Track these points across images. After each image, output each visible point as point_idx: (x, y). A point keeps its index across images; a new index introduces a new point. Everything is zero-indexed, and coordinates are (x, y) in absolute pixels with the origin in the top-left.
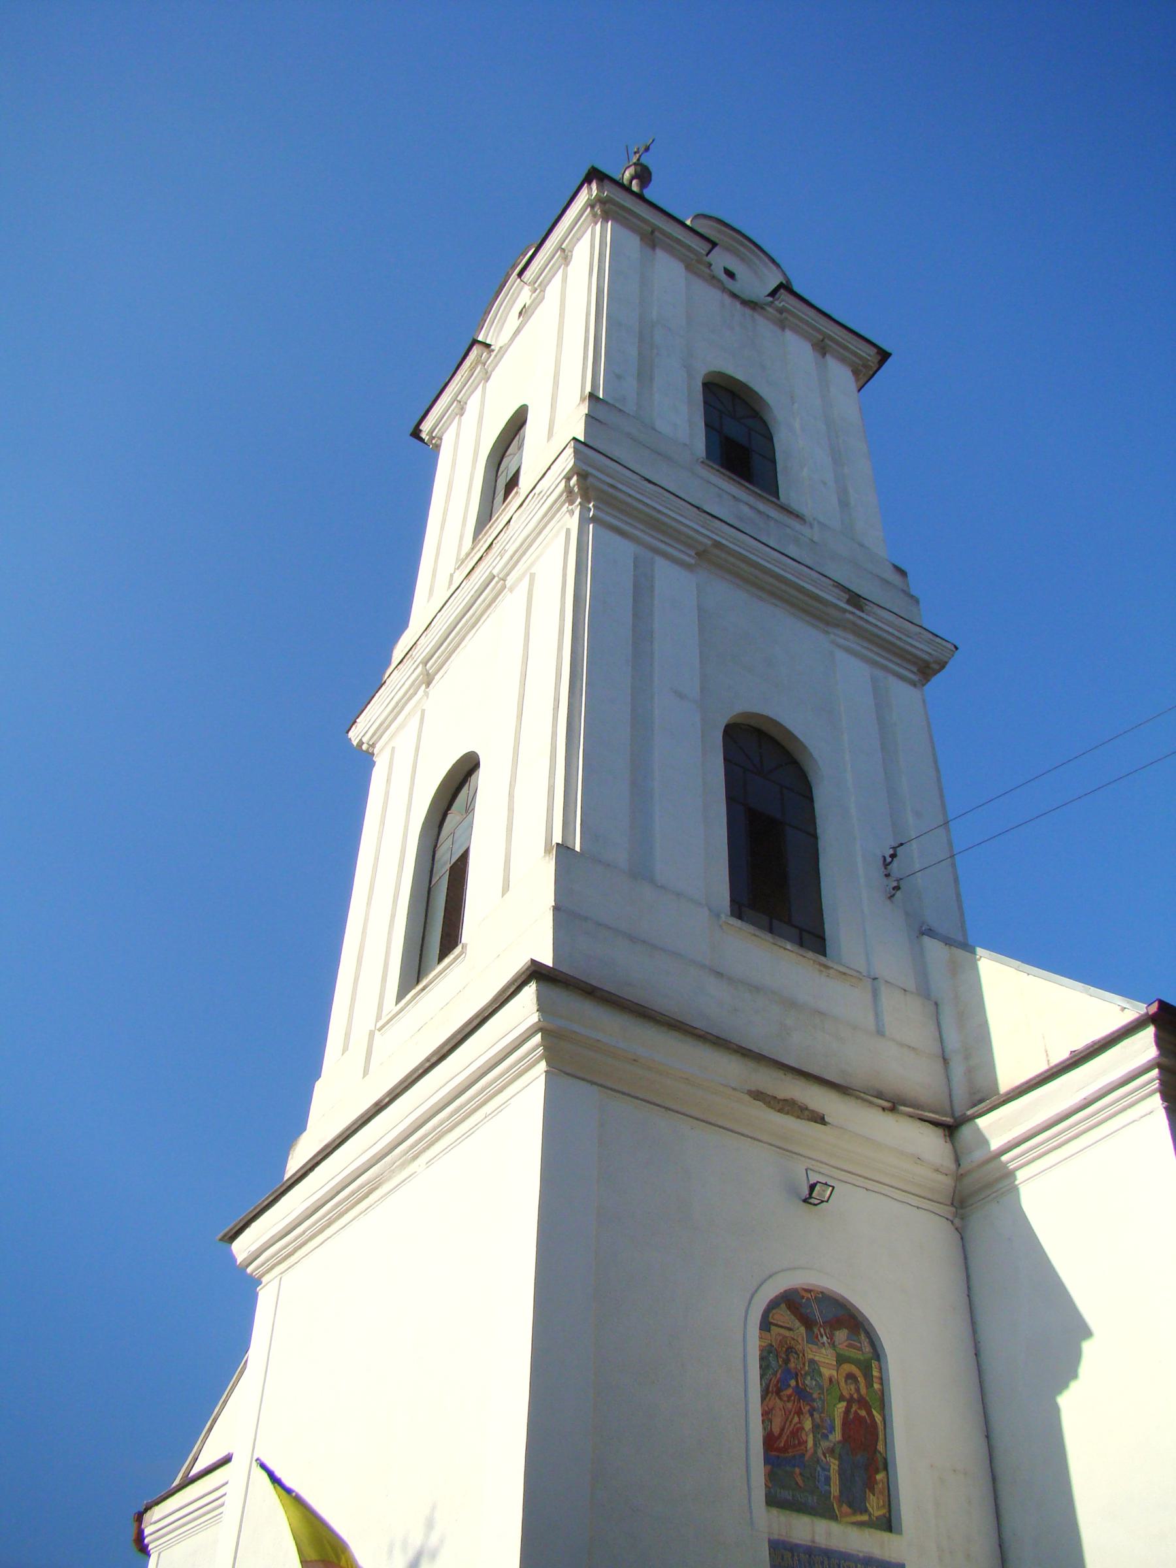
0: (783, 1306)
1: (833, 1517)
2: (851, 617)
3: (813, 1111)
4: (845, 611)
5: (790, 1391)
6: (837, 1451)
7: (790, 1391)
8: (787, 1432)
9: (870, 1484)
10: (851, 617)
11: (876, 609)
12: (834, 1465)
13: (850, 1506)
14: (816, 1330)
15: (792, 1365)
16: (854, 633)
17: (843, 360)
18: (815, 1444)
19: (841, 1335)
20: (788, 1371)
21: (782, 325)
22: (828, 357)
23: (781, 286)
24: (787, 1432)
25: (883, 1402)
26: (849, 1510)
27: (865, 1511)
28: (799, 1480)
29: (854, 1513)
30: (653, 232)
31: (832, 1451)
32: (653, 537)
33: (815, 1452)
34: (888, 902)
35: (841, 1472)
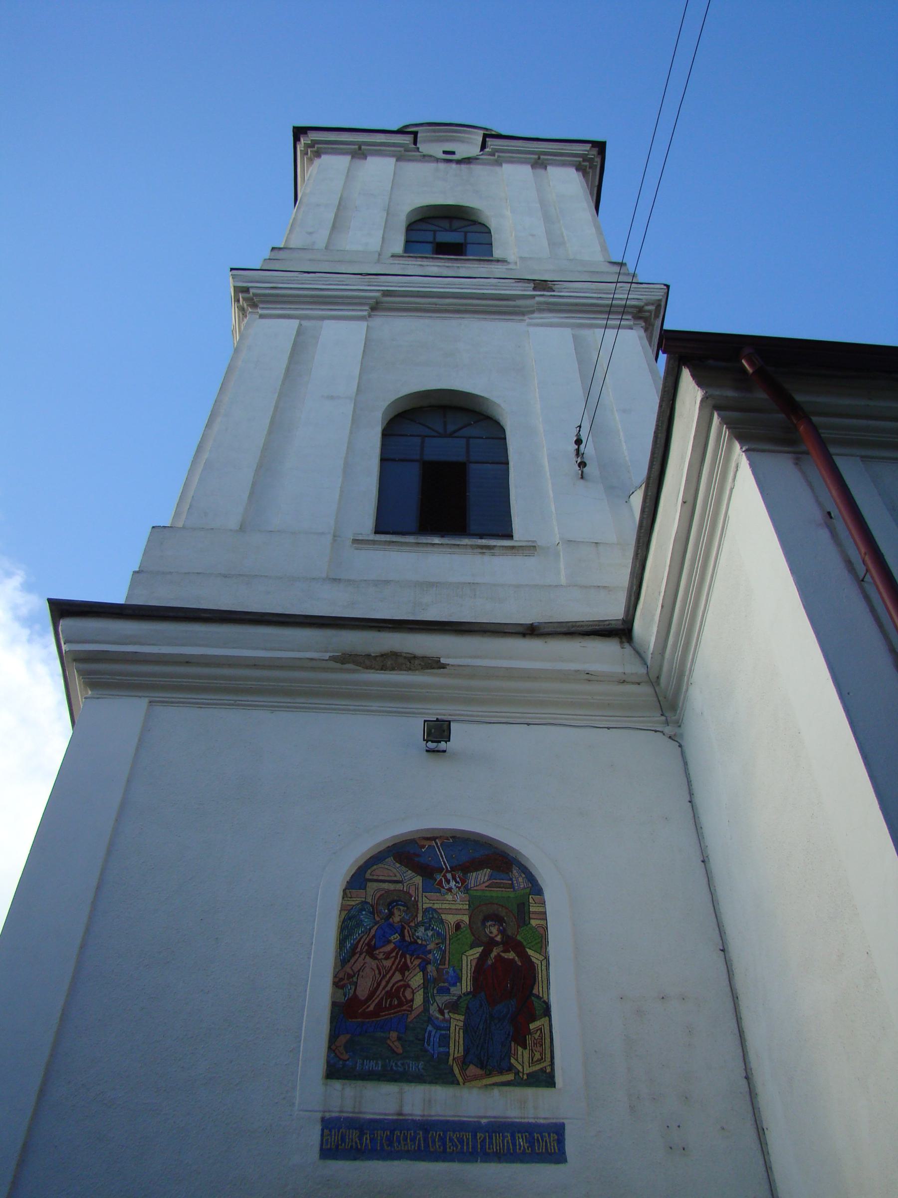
0: (390, 860)
1: (454, 1082)
2: (541, 299)
3: (423, 658)
4: (533, 297)
5: (390, 947)
6: (463, 1005)
7: (390, 947)
8: (380, 993)
9: (520, 1037)
10: (541, 299)
11: (566, 285)
12: (457, 1021)
13: (482, 1066)
14: (439, 877)
15: (396, 919)
16: (550, 311)
17: (564, 164)
18: (426, 1001)
19: (480, 878)
20: (391, 926)
21: (498, 163)
22: (549, 168)
23: (485, 136)
24: (380, 993)
25: (541, 940)
26: (479, 1072)
27: (510, 1068)
28: (398, 1047)
29: (489, 1075)
30: (360, 149)
31: (454, 1007)
32: (323, 310)
33: (426, 1009)
34: (582, 481)
35: (467, 1028)
